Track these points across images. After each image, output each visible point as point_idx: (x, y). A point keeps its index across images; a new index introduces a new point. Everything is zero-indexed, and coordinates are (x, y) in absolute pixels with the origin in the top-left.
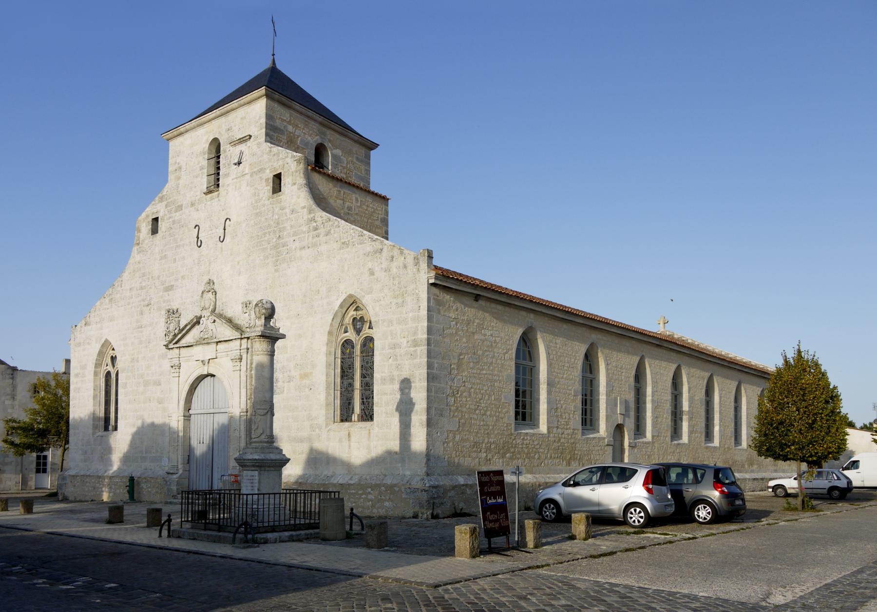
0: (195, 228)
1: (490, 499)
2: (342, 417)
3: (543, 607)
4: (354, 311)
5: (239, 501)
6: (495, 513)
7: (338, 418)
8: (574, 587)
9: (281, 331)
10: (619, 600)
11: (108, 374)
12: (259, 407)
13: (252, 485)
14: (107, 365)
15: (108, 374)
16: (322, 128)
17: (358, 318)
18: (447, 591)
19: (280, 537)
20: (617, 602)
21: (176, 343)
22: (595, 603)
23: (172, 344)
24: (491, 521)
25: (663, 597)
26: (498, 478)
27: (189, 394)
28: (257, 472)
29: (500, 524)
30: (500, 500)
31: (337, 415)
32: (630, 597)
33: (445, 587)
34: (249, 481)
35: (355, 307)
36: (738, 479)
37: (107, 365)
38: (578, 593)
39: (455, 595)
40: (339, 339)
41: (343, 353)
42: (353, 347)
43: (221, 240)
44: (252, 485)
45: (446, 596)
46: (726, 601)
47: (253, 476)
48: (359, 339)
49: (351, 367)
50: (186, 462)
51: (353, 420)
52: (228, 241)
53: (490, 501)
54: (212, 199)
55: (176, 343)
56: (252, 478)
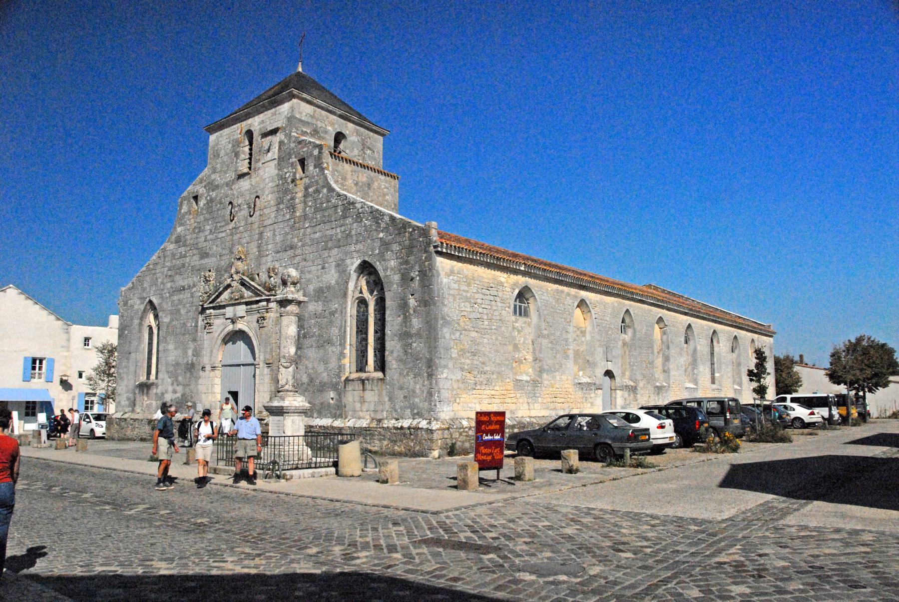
1: (487, 435)
3: (529, 528)
6: (491, 448)
8: (556, 511)
9: (853, 341)
10: (593, 520)
18: (447, 517)
19: (304, 474)
20: (591, 522)
21: (210, 303)
22: (572, 523)
24: (483, 454)
25: (630, 517)
26: (499, 418)
29: (493, 457)
30: (497, 437)
32: (602, 518)
33: (446, 514)
36: (284, 419)
38: (559, 516)
39: (455, 520)
45: (448, 521)
46: (681, 518)
49: (366, 321)
53: (486, 438)
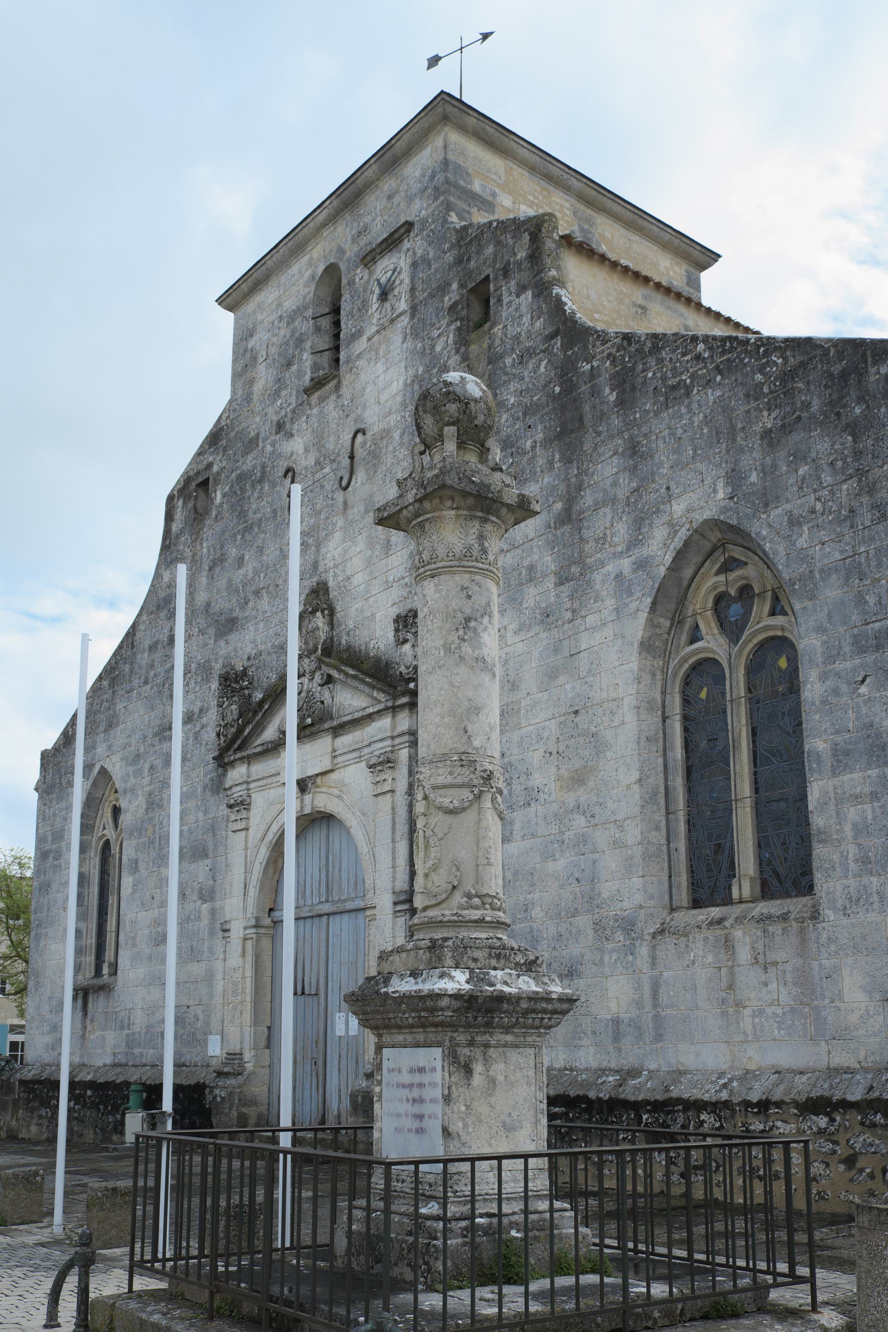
0: (285, 476)
2: (694, 891)
4: (717, 573)
5: (333, 1221)
7: (683, 896)
11: (107, 844)
12: (441, 780)
13: (417, 1109)
14: (104, 828)
15: (107, 844)
16: (583, 208)
17: (733, 592)
23: (231, 752)
27: (271, 871)
28: (437, 1052)
31: (679, 886)
34: (404, 1093)
35: (722, 559)
37: (104, 828)
40: (672, 665)
41: (686, 701)
42: (720, 679)
43: (344, 483)
44: (417, 1109)
47: (421, 1070)
48: (740, 652)
50: (263, 1042)
51: (735, 894)
52: (359, 483)
54: (322, 399)
55: (240, 748)
56: (417, 1078)
